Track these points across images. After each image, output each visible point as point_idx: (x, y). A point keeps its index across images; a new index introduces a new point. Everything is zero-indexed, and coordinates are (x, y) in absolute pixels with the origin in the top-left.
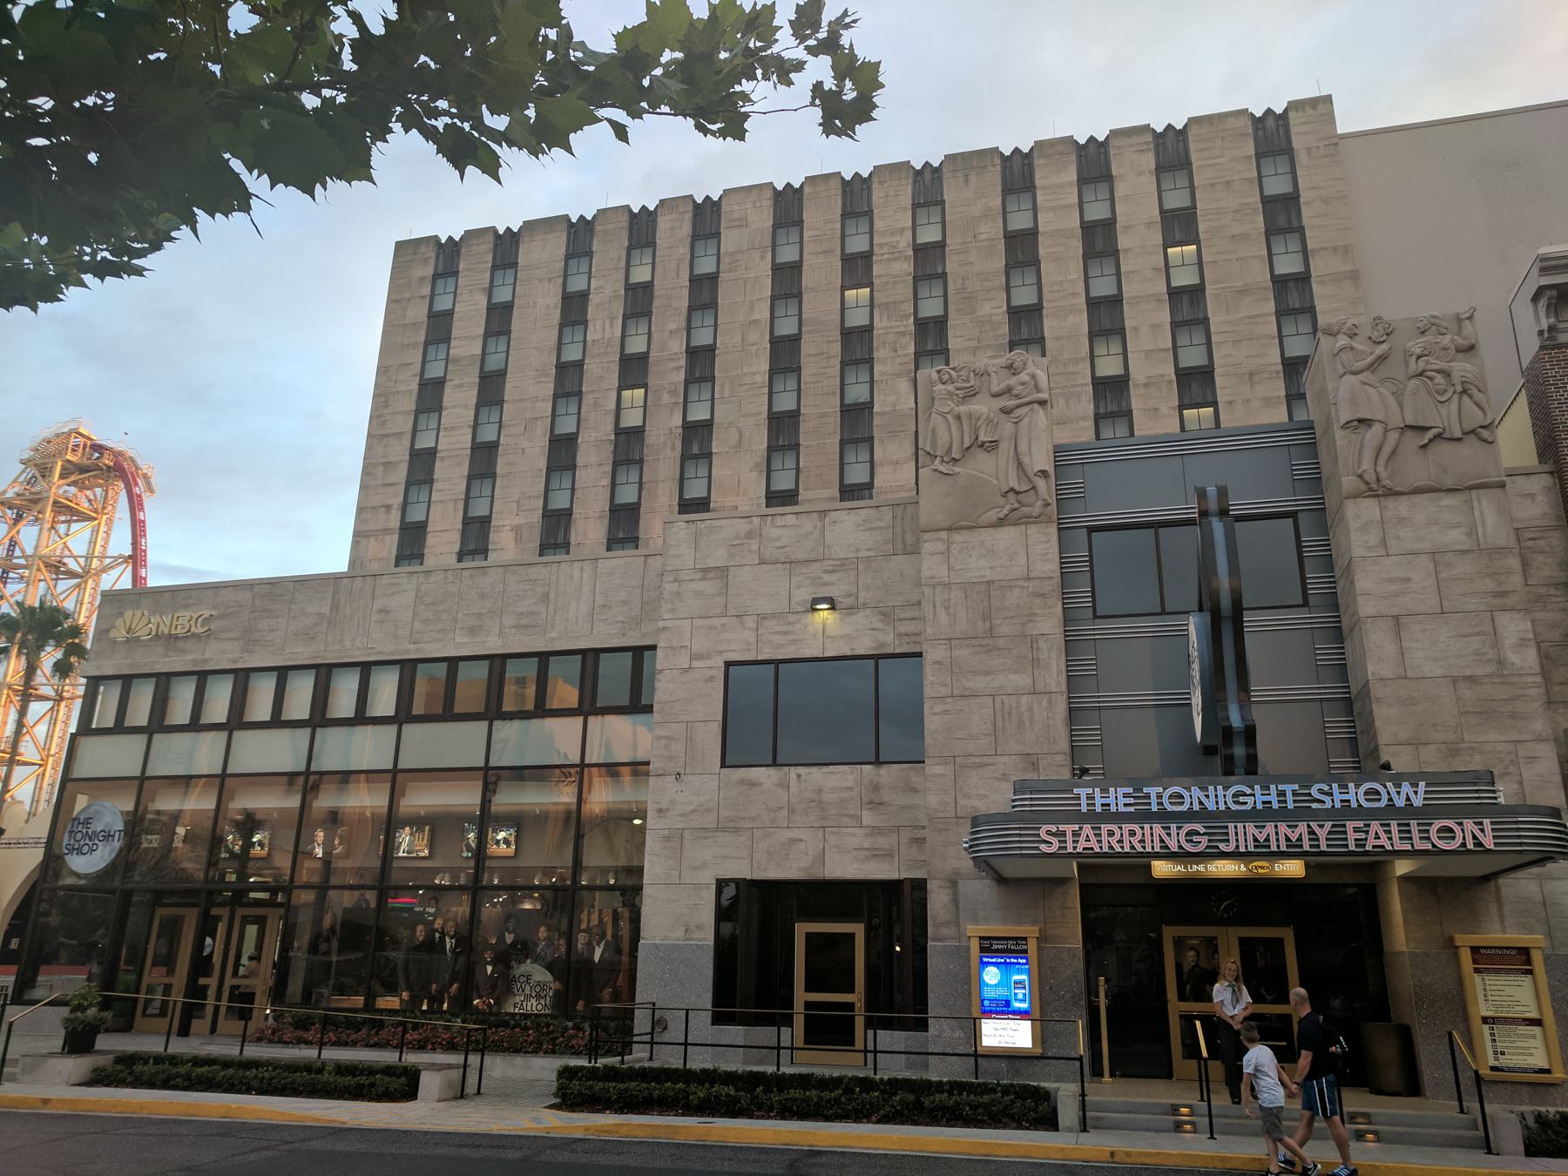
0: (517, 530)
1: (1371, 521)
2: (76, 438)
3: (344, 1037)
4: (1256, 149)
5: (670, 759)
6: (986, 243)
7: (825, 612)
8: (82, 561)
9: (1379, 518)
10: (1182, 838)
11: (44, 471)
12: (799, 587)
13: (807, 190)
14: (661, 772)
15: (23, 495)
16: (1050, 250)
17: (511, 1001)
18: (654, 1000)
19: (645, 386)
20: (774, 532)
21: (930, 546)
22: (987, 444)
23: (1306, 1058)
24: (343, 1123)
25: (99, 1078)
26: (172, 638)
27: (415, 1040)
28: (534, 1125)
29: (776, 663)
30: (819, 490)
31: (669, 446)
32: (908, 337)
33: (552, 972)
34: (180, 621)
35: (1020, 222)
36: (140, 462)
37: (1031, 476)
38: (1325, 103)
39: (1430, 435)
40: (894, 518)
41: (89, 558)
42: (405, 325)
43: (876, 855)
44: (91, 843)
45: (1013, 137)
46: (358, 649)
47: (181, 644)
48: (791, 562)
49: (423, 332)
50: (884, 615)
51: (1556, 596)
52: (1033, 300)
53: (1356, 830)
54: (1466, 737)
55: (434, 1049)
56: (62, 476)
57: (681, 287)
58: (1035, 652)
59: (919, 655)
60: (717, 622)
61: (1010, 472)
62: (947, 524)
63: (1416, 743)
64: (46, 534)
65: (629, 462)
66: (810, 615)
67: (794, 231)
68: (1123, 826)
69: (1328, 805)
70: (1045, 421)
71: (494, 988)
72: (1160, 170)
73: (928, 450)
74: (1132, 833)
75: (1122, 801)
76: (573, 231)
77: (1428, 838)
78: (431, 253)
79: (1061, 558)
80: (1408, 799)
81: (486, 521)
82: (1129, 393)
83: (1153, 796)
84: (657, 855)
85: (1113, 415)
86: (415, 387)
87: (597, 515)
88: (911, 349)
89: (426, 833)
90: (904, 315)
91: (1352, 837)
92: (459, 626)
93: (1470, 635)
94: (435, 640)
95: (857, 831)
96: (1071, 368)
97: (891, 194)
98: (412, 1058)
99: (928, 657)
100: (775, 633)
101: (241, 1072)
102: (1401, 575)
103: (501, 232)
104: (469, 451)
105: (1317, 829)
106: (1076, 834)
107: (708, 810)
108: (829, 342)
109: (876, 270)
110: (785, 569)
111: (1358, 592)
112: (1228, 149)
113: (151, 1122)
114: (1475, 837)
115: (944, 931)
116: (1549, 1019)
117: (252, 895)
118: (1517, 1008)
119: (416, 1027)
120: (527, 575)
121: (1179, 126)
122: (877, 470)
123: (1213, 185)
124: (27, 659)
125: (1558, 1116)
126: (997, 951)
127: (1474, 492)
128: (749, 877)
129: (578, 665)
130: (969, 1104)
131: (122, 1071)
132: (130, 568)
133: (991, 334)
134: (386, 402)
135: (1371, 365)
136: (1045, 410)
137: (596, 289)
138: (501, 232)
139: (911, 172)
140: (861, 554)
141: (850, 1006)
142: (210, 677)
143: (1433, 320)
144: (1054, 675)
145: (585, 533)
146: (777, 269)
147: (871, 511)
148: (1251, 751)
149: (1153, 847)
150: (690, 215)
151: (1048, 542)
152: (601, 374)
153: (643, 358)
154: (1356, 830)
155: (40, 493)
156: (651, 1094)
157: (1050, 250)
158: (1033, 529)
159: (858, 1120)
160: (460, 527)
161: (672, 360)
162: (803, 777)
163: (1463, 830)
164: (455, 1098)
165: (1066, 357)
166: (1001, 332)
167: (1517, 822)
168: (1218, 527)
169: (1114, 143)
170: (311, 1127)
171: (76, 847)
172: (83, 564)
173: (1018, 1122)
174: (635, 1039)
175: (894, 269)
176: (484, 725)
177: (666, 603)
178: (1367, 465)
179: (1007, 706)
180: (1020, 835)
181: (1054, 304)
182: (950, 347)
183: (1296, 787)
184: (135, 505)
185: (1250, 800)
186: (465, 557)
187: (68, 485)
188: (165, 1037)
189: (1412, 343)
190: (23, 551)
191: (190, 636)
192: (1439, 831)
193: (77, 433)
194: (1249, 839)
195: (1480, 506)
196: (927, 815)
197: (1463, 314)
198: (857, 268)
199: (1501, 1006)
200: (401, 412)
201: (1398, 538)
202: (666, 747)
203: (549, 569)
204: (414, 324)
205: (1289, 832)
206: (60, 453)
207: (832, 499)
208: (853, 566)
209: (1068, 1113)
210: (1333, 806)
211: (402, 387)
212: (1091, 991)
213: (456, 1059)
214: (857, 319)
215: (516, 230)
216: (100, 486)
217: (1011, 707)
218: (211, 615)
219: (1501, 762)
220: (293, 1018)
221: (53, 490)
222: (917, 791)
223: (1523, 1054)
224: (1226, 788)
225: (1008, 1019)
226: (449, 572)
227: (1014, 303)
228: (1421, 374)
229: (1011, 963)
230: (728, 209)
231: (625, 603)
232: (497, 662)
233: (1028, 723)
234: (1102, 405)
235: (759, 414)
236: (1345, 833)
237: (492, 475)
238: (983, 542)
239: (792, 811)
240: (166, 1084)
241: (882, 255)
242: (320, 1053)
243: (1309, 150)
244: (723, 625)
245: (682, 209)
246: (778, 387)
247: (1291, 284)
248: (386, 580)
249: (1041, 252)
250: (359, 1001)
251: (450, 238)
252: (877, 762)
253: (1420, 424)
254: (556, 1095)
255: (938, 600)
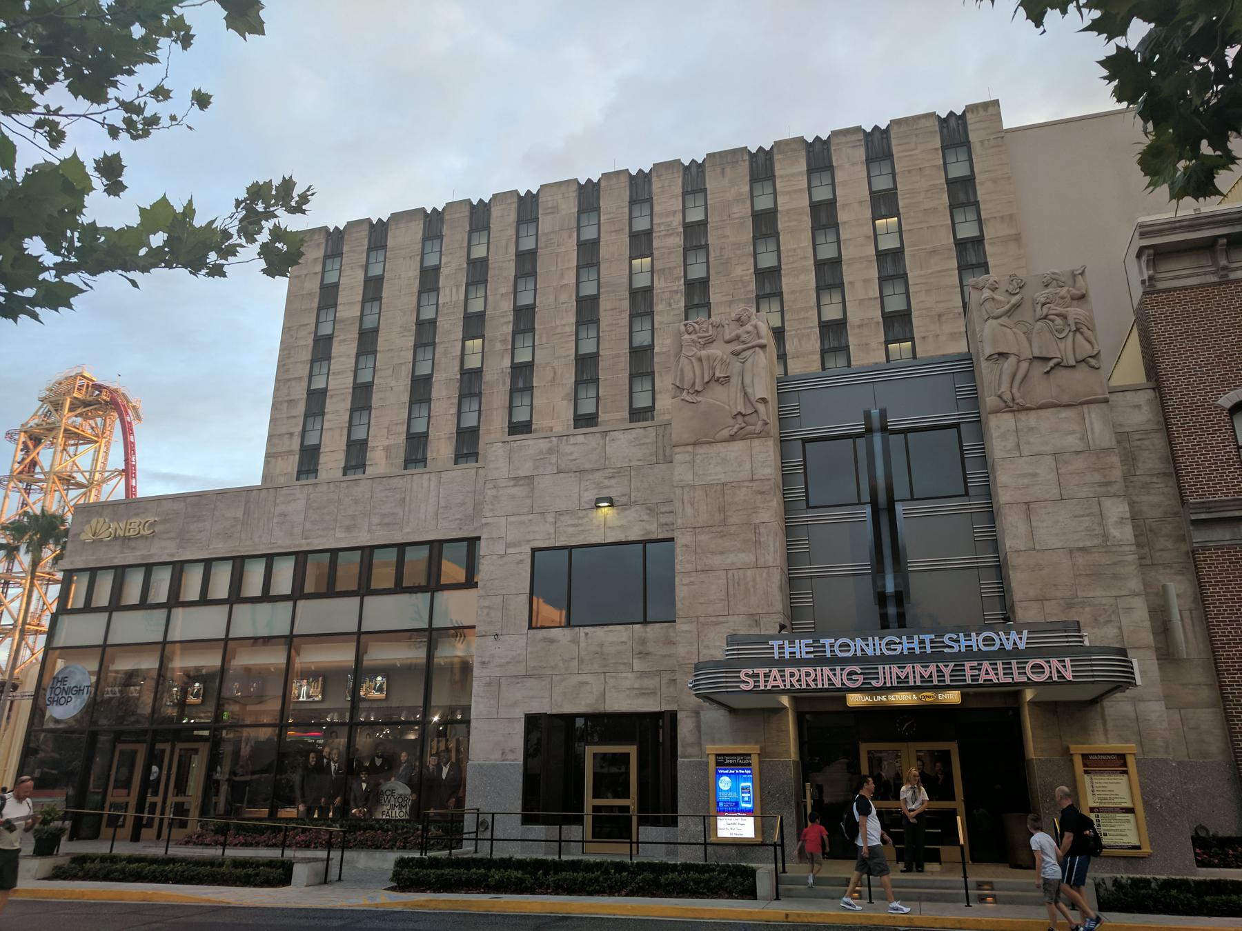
0: (387, 449)
1: (1008, 431)
2: (80, 380)
3: (250, 839)
4: (942, 143)
5: (491, 623)
6: (738, 221)
7: (606, 509)
8: (87, 475)
9: (1014, 427)
10: (845, 677)
11: (57, 406)
12: (586, 490)
13: (603, 184)
14: (484, 633)
15: (42, 425)
16: (787, 224)
17: (380, 810)
18: (478, 807)
19: (483, 337)
20: (569, 449)
21: (681, 456)
22: (722, 379)
23: (1069, 838)
24: (229, 903)
25: (58, 874)
26: (126, 539)
27: (303, 841)
28: (368, 902)
29: (570, 548)
30: (613, 413)
31: (501, 382)
32: (680, 294)
33: (409, 786)
34: (132, 526)
35: (764, 203)
36: (130, 397)
37: (754, 402)
38: (994, 106)
39: (1051, 364)
40: (657, 435)
41: (92, 472)
42: (302, 295)
43: (644, 693)
44: (66, 697)
45: (814, 128)
46: (264, 544)
47: (133, 544)
48: (581, 472)
49: (316, 300)
50: (650, 510)
51: (1157, 483)
52: (774, 263)
53: (972, 668)
54: (1079, 594)
55: (316, 848)
56: (71, 410)
57: (510, 261)
58: (757, 535)
59: (672, 540)
60: (523, 518)
61: (738, 402)
62: (692, 440)
63: (1041, 599)
64: (59, 455)
65: (471, 395)
66: (595, 511)
67: (594, 215)
68: (801, 669)
69: (956, 650)
70: (764, 361)
71: (367, 800)
72: (869, 161)
73: (678, 384)
74: (808, 674)
75: (804, 650)
76: (428, 219)
77: (1025, 673)
78: (322, 239)
79: (782, 463)
80: (1015, 643)
81: (364, 443)
82: (847, 332)
83: (828, 646)
84: (482, 697)
85: (835, 350)
86: (310, 341)
87: (447, 436)
88: (682, 304)
89: (320, 683)
90: (677, 278)
91: (968, 673)
92: (338, 525)
93: (1083, 516)
94: (321, 536)
95: (630, 675)
96: (802, 315)
97: (666, 184)
98: (289, 853)
99: (678, 542)
100: (569, 526)
101: (162, 867)
102: (1031, 471)
103: (429, 212)
104: (351, 390)
105: (942, 668)
106: (766, 676)
107: (519, 662)
108: (620, 300)
109: (655, 244)
110: (576, 477)
111: (999, 485)
112: (920, 143)
113: (87, 905)
114: (1058, 672)
115: (690, 750)
116: (1140, 808)
117: (196, 733)
118: (1116, 800)
119: (304, 831)
120: (389, 484)
121: (883, 127)
122: (657, 396)
123: (909, 171)
124: (33, 555)
125: (1129, 881)
126: (729, 764)
127: (1086, 406)
128: (549, 712)
129: (395, 555)
130: (693, 880)
131: (75, 868)
132: (123, 479)
133: (742, 290)
134: (289, 354)
135: (1008, 311)
136: (765, 352)
137: (445, 264)
138: (429, 212)
139: (681, 168)
140: (633, 464)
141: (626, 809)
142: (214, 563)
143: (1054, 276)
144: (773, 551)
145: (438, 450)
146: (581, 245)
147: (641, 431)
148: (901, 610)
149: (823, 685)
150: (515, 205)
151: (767, 452)
152: (450, 327)
153: (481, 315)
154: (972, 668)
155: (54, 423)
156: (461, 878)
157: (787, 224)
158: (756, 442)
159: (611, 894)
160: (345, 448)
161: (503, 316)
162: (589, 635)
163: (1050, 667)
164: (320, 884)
165: (799, 306)
166: (749, 289)
167: (1091, 660)
168: (877, 438)
169: (834, 141)
170: (586, 918)
171: (56, 699)
172: (88, 477)
173: (730, 894)
174: (465, 836)
175: (669, 243)
176: (357, 600)
177: (487, 504)
178: (1004, 387)
179: (736, 577)
180: (726, 677)
181: (790, 266)
182: (711, 301)
183: (933, 636)
184: (127, 430)
185: (899, 647)
186: (348, 472)
187: (76, 416)
188: (111, 842)
189: (1039, 294)
190: (42, 468)
191: (139, 537)
192: (1032, 667)
193: (81, 376)
194: (894, 677)
195: (1090, 417)
196: (678, 662)
197: (1077, 270)
198: (641, 243)
199: (1105, 799)
200: (301, 362)
201: (1028, 443)
202: (488, 614)
203: (405, 480)
204: (310, 294)
205: (922, 670)
206: (69, 392)
207: (623, 420)
208: (627, 473)
209: (764, 884)
210: (960, 651)
211: (301, 343)
212: (801, 793)
213: (322, 854)
214: (642, 281)
215: (385, 221)
216: (99, 416)
217: (739, 579)
218: (155, 521)
219: (1106, 612)
220: (214, 826)
221: (64, 421)
222: (674, 644)
223: (1121, 835)
224: (881, 639)
225: (737, 816)
226: (331, 485)
227: (760, 266)
228: (1045, 318)
229: (739, 774)
230: (544, 199)
231: (462, 504)
232: (367, 552)
233: (752, 590)
234: (826, 342)
235: (568, 356)
236: (964, 670)
237: (369, 408)
238: (719, 453)
239: (581, 661)
240: (107, 877)
241: (660, 232)
242: (283, 853)
243: (982, 142)
244: (530, 520)
245: (509, 201)
246: (583, 335)
247: (969, 246)
248: (284, 491)
249: (780, 226)
250: (265, 812)
251: (380, 220)
252: (645, 622)
253: (1044, 355)
254: (392, 880)
255: (686, 497)
